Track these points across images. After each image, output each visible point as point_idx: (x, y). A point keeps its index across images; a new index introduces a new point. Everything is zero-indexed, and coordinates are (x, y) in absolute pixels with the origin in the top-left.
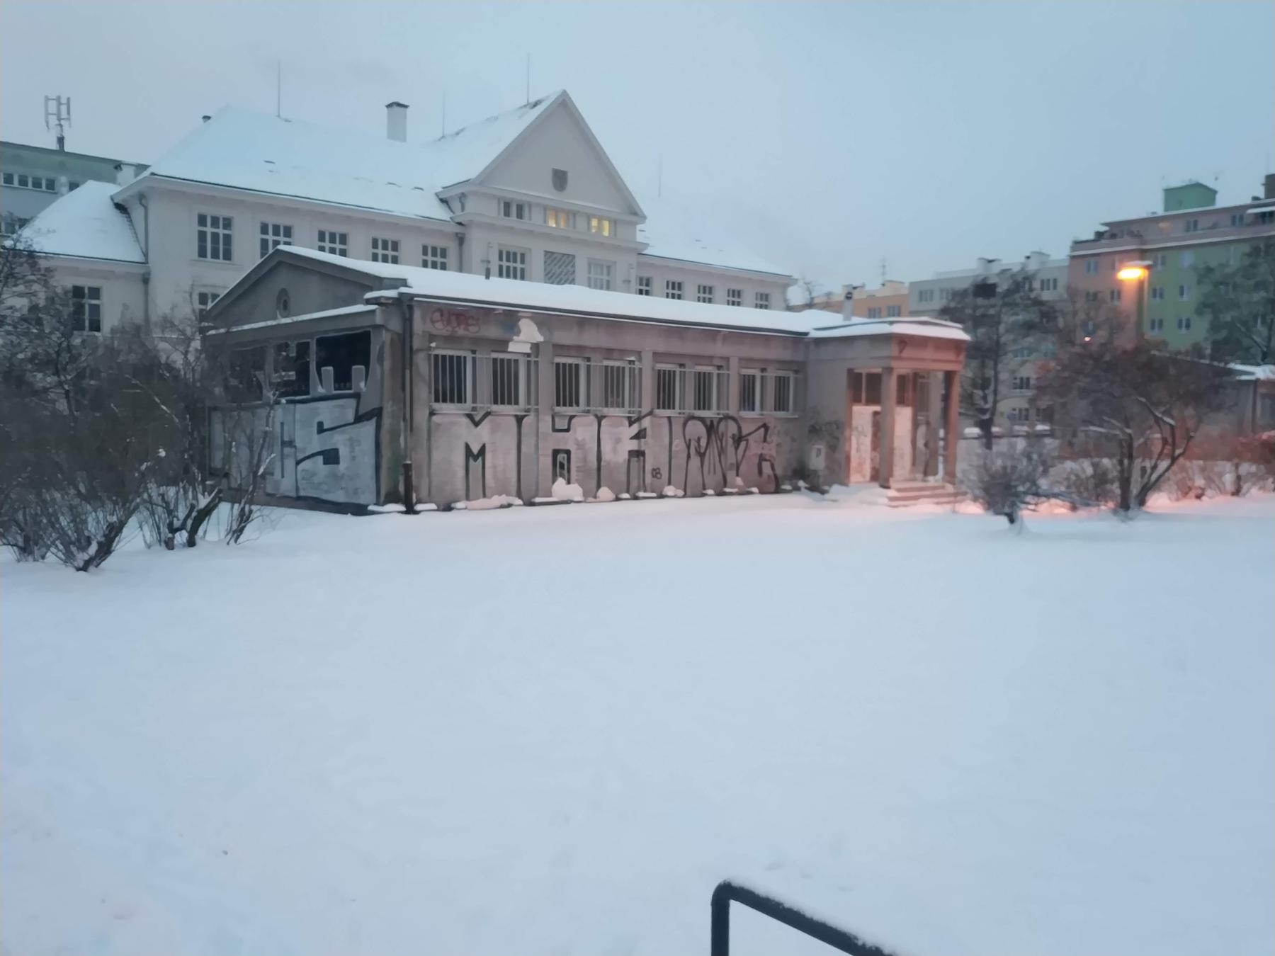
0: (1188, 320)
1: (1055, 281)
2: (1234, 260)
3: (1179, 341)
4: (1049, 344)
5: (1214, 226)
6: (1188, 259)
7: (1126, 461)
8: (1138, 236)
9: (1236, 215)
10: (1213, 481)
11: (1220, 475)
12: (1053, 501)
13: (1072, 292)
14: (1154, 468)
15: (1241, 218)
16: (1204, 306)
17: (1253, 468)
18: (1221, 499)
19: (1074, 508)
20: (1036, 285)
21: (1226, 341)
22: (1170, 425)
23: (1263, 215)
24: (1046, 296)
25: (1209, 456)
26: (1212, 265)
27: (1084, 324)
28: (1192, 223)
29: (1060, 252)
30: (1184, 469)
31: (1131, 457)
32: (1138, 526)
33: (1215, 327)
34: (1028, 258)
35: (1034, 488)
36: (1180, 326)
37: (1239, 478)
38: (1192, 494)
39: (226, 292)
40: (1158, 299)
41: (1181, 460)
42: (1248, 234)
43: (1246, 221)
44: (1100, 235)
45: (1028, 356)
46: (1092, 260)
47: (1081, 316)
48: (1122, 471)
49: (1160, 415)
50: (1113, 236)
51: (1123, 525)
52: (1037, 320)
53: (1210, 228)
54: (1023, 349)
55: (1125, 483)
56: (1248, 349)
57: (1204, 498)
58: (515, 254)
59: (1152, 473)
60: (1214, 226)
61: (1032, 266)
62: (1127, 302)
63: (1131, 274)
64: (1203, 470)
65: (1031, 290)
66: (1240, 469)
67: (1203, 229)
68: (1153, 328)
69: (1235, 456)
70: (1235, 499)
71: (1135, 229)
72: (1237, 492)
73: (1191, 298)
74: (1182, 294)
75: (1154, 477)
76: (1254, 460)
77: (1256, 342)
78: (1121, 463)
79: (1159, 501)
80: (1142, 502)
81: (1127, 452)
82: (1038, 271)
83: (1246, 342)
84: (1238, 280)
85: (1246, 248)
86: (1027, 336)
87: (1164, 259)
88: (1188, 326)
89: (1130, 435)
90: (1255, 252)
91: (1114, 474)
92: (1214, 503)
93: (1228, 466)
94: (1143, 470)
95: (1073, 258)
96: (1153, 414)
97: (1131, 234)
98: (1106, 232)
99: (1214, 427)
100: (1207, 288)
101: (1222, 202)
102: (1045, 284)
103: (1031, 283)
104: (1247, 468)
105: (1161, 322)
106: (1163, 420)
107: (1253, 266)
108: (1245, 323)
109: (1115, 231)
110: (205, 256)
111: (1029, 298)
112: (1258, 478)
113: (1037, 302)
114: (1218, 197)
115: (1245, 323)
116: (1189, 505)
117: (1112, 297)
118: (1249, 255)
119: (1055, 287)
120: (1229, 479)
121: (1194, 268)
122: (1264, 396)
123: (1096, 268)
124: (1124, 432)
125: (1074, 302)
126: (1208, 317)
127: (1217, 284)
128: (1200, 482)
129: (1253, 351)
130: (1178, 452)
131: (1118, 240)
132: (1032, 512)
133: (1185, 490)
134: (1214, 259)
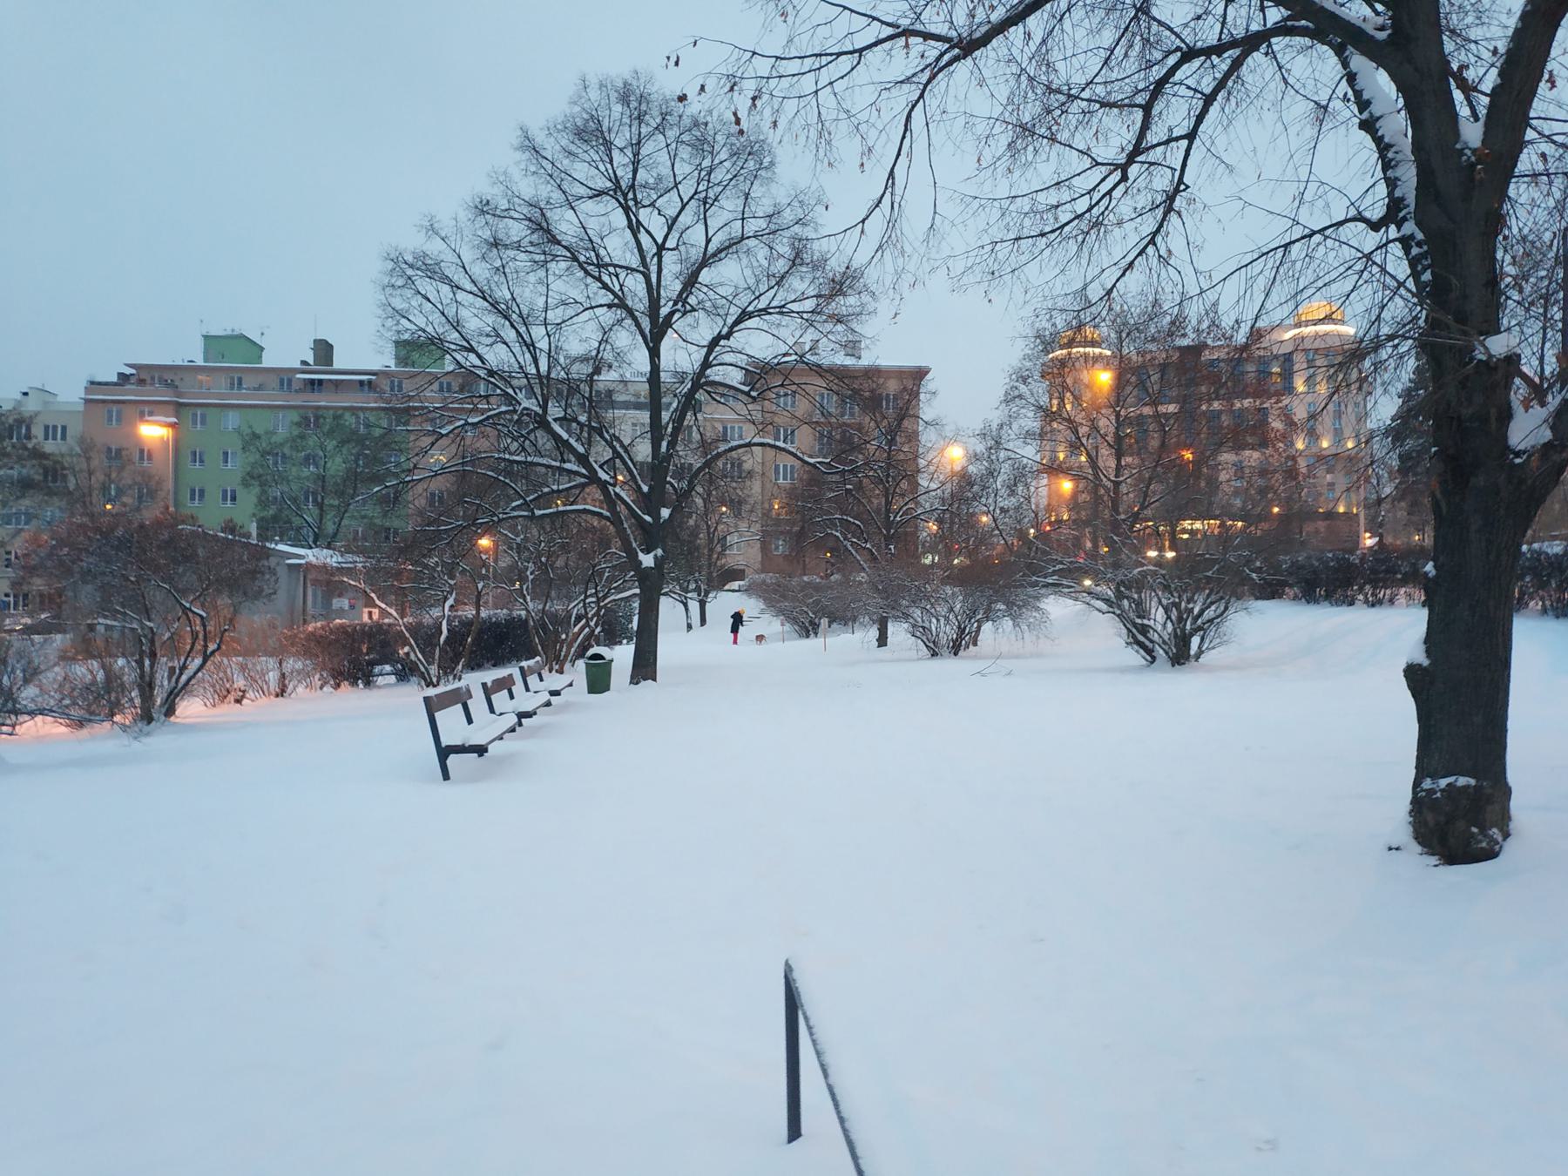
0: (234, 493)
1: (64, 428)
2: (283, 428)
3: (211, 516)
4: (53, 510)
5: (260, 388)
6: (232, 420)
7: (147, 662)
8: (171, 385)
9: (284, 377)
10: (256, 681)
11: (263, 674)
12: (39, 718)
13: (87, 447)
14: (183, 668)
15: (290, 381)
16: (249, 478)
17: (299, 665)
18: (264, 701)
19: (80, 724)
20: (38, 431)
21: (275, 518)
22: (201, 616)
23: (312, 382)
24: (50, 447)
25: (248, 652)
26: (258, 431)
27: (105, 489)
28: (236, 380)
29: (71, 394)
30: (219, 667)
31: (153, 655)
32: (160, 740)
33: (263, 502)
34: (25, 394)
35: (10, 705)
36: (225, 499)
37: (283, 676)
38: (231, 698)
39: (889, 633)
40: (50, 441)
41: (217, 658)
42: (297, 401)
43: (295, 386)
44: (123, 378)
45: (25, 524)
46: (115, 408)
47: (99, 477)
48: (142, 676)
49: (188, 605)
50: (142, 382)
51: (136, 744)
52: (38, 478)
53: (255, 389)
54: (18, 514)
55: (147, 687)
56: (299, 529)
57: (245, 701)
58: (55, 428)
59: (181, 674)
60: (260, 388)
61: (31, 406)
62: (163, 467)
63: (153, 432)
64: (243, 668)
65: (29, 437)
66: (284, 664)
67: (248, 389)
68: (192, 498)
69: (279, 653)
70: (280, 699)
71: (168, 376)
72: (281, 693)
73: (237, 466)
74: (226, 461)
75: (184, 678)
76: (297, 655)
77: (307, 522)
78: (140, 663)
79: (191, 708)
80: (170, 711)
81: (146, 649)
82: (37, 414)
83: (297, 521)
84: (287, 451)
85: (295, 416)
86: (23, 496)
87: (203, 417)
88: (234, 499)
89: (151, 628)
90: (304, 422)
91: (130, 677)
92: (258, 707)
93: (272, 662)
94: (172, 670)
95: (87, 401)
96: (181, 604)
97: (164, 382)
98: (132, 375)
99: (255, 618)
100: (254, 457)
101: (268, 362)
102: (49, 432)
103: (28, 429)
104: (292, 664)
105: (202, 492)
106: (190, 610)
107: (302, 437)
108: (295, 500)
109: (140, 374)
110: (200, 490)
111: (26, 448)
112: (304, 675)
113: (38, 454)
114: (264, 354)
115: (295, 500)
116: (229, 710)
117: (142, 458)
118: (298, 424)
119: (64, 437)
120: (273, 677)
121: (238, 431)
122: (316, 582)
123: (119, 419)
124: (143, 627)
125: (88, 459)
126: (256, 490)
127: (264, 454)
128: (240, 683)
129: (304, 531)
130: (212, 647)
131: (148, 388)
132: (8, 737)
133: (223, 694)
134: (261, 424)
